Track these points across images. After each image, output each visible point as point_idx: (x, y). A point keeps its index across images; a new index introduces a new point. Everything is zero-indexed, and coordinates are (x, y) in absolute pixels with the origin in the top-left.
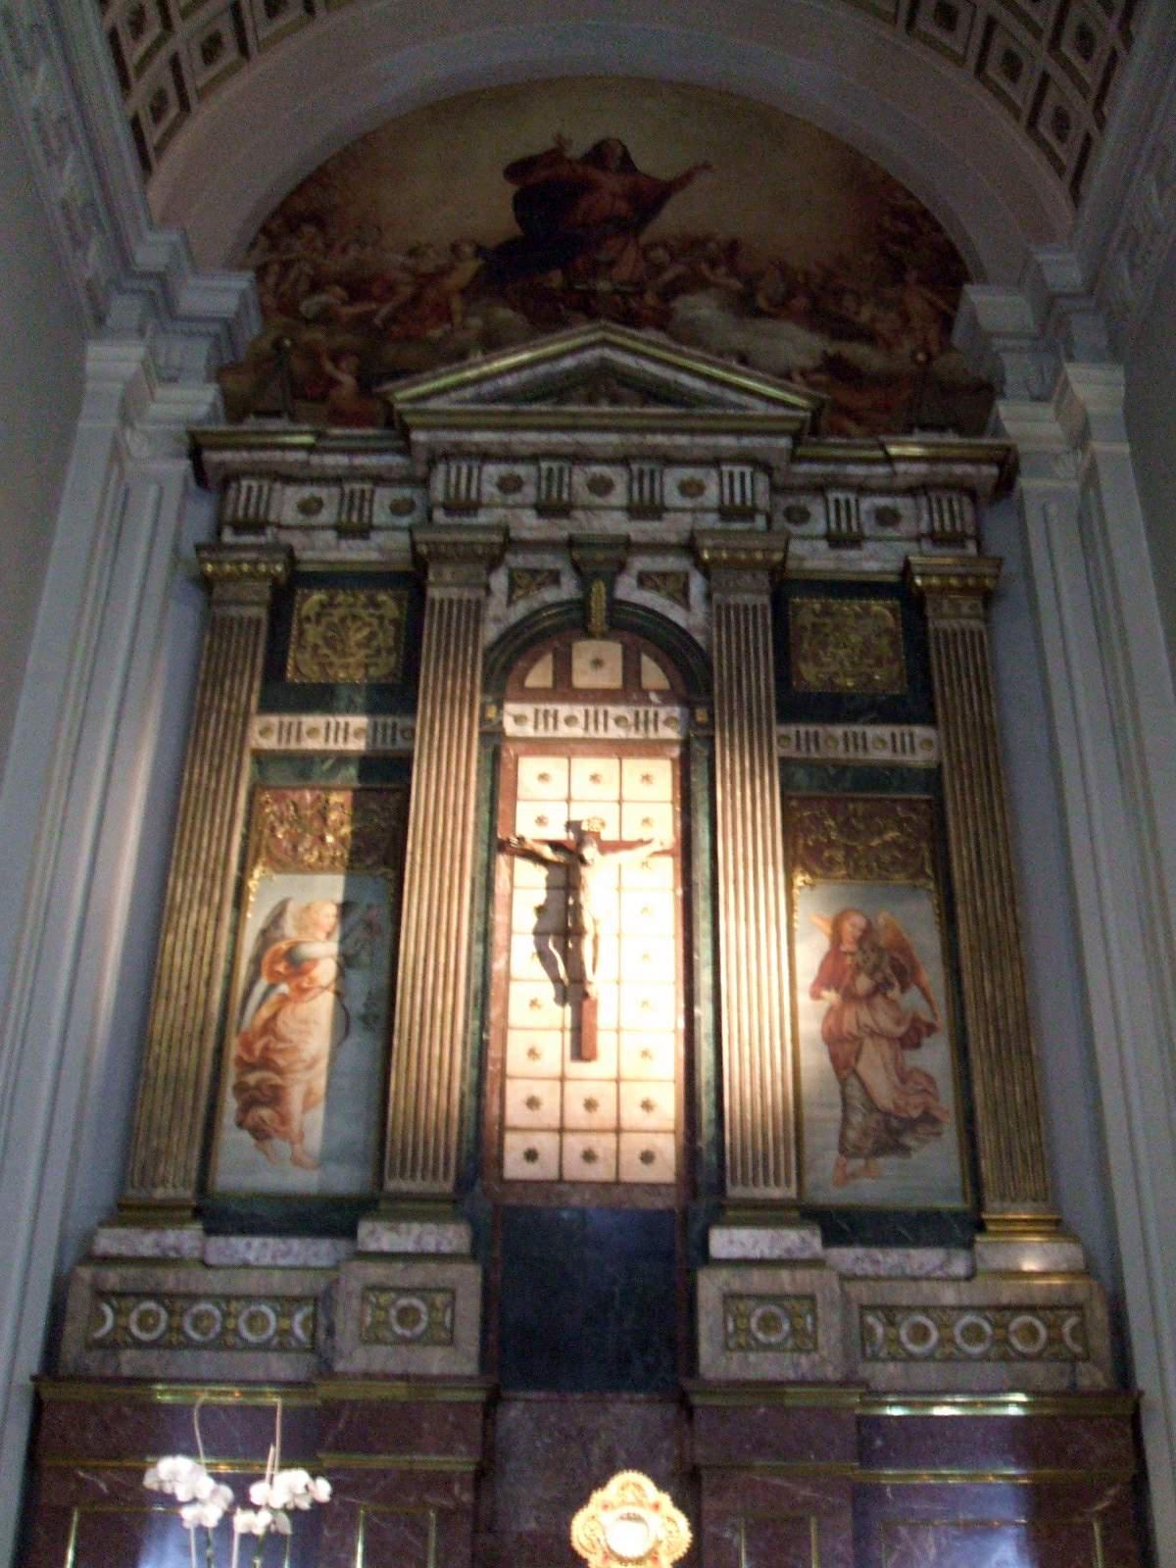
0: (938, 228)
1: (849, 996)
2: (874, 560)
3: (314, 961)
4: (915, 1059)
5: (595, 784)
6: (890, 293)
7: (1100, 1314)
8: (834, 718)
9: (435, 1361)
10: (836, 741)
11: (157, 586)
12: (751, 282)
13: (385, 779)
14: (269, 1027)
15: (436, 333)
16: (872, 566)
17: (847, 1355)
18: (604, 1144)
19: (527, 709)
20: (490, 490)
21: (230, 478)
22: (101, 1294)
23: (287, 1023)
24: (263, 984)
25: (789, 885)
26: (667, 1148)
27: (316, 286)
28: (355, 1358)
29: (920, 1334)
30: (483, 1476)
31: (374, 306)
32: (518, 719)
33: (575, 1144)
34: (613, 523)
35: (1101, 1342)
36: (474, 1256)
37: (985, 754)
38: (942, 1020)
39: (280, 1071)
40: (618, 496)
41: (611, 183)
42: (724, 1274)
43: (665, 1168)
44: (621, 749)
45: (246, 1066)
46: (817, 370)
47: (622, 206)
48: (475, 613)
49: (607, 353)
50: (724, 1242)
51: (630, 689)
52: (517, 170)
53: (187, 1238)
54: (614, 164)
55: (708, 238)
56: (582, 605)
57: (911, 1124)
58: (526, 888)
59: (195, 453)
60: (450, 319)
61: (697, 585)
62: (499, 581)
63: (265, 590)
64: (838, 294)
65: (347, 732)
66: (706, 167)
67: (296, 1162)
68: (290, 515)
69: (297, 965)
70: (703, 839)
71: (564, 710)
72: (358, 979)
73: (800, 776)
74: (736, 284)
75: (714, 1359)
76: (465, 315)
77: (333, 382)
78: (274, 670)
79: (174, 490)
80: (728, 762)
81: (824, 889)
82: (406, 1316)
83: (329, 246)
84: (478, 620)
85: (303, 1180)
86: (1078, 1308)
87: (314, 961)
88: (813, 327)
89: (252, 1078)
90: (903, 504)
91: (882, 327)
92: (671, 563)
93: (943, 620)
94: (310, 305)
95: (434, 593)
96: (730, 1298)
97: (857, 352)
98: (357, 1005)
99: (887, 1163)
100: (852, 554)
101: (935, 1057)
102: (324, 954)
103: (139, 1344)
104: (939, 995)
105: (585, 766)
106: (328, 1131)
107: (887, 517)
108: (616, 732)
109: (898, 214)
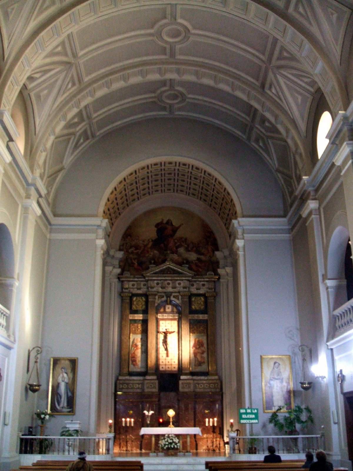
1: (196, 348)
2: (202, 292)
4: (203, 355)
5: (168, 324)
7: (219, 384)
10: (196, 317)
11: (116, 297)
13: (145, 323)
14: (134, 353)
15: (147, 255)
18: (170, 366)
20: (155, 285)
21: (123, 281)
22: (120, 384)
23: (136, 353)
24: (133, 348)
25: (190, 335)
26: (177, 367)
27: (131, 247)
28: (146, 390)
30: (159, 401)
32: (160, 316)
33: (167, 366)
35: (219, 386)
38: (206, 351)
40: (171, 285)
41: (169, 227)
43: (176, 369)
44: (172, 320)
48: (154, 302)
50: (182, 377)
51: (172, 312)
52: (157, 225)
53: (128, 377)
58: (161, 337)
59: (119, 278)
61: (180, 297)
62: (157, 297)
63: (129, 298)
65: (140, 317)
67: (138, 368)
69: (136, 346)
70: (180, 331)
71: (165, 315)
72: (143, 348)
73: (192, 321)
74: (186, 246)
75: (181, 389)
77: (134, 264)
78: (131, 308)
80: (183, 322)
81: (194, 335)
84: (155, 303)
85: (139, 370)
86: (217, 383)
88: (196, 253)
89: (133, 359)
93: (211, 300)
94: (130, 251)
95: (150, 300)
96: (182, 383)
98: (143, 350)
99: (199, 367)
101: (205, 355)
102: (139, 344)
104: (206, 348)
106: (141, 365)
107: (203, 285)
108: (171, 318)
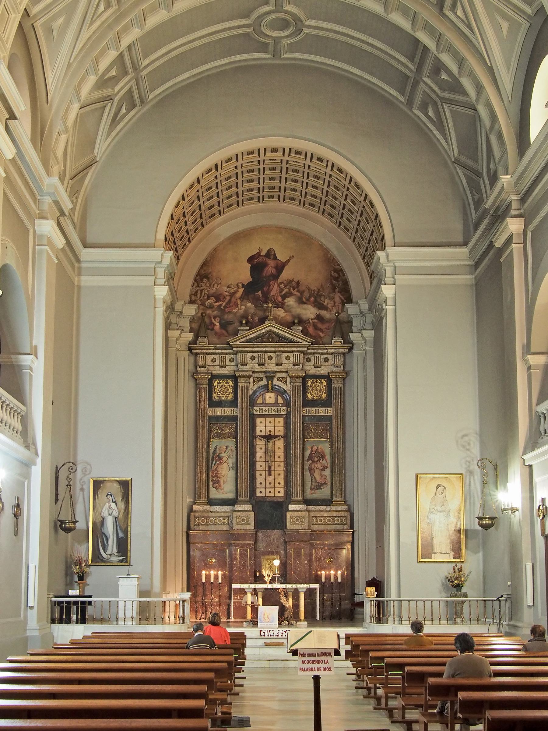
0: (344, 275)
2: (322, 371)
3: (223, 457)
6: (332, 295)
8: (313, 407)
9: (248, 527)
12: (302, 293)
15: (235, 311)
16: (322, 372)
17: (309, 524)
19: (257, 408)
21: (196, 354)
22: (195, 517)
24: (214, 461)
27: (208, 298)
29: (321, 521)
31: (221, 303)
34: (272, 368)
36: (253, 511)
37: (342, 414)
39: (218, 477)
41: (271, 263)
42: (291, 512)
45: (213, 477)
46: (315, 319)
47: (274, 271)
49: (271, 328)
50: (291, 507)
54: (272, 257)
55: (293, 280)
56: (267, 386)
57: (322, 485)
59: (190, 349)
60: (238, 307)
61: (289, 380)
62: (251, 380)
64: (320, 296)
66: (293, 257)
68: (210, 362)
71: (264, 408)
74: (298, 294)
75: (289, 526)
76: (241, 305)
79: (187, 358)
82: (243, 520)
83: (210, 285)
87: (223, 457)
90: (329, 356)
91: (329, 306)
92: (284, 375)
94: (207, 303)
97: (324, 313)
100: (319, 369)
103: (202, 525)
104: (329, 462)
105: (268, 420)
107: (326, 360)
109: (336, 271)
